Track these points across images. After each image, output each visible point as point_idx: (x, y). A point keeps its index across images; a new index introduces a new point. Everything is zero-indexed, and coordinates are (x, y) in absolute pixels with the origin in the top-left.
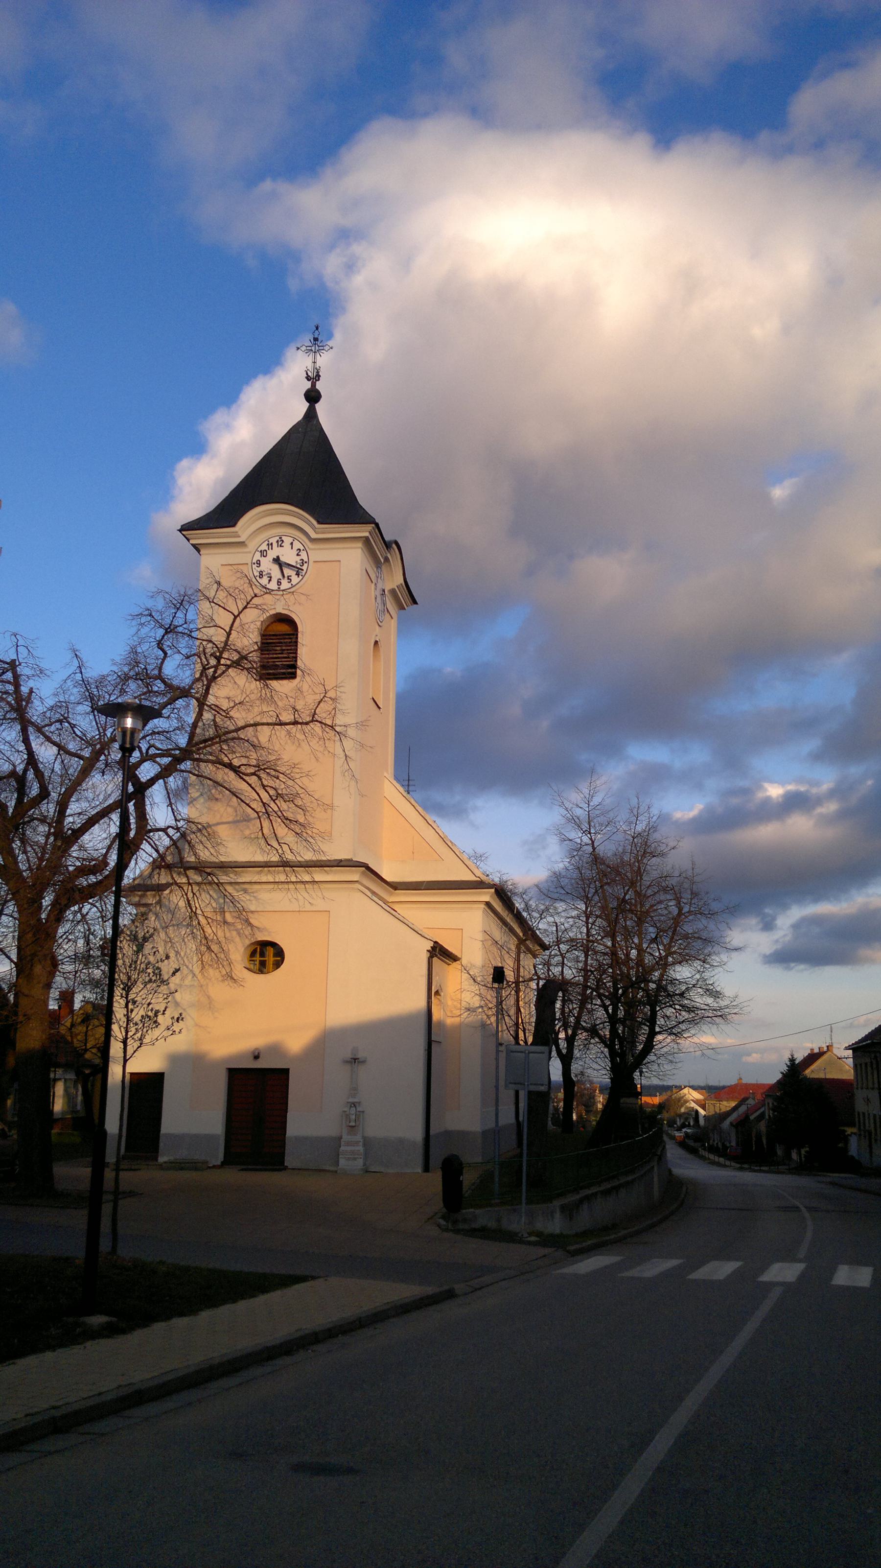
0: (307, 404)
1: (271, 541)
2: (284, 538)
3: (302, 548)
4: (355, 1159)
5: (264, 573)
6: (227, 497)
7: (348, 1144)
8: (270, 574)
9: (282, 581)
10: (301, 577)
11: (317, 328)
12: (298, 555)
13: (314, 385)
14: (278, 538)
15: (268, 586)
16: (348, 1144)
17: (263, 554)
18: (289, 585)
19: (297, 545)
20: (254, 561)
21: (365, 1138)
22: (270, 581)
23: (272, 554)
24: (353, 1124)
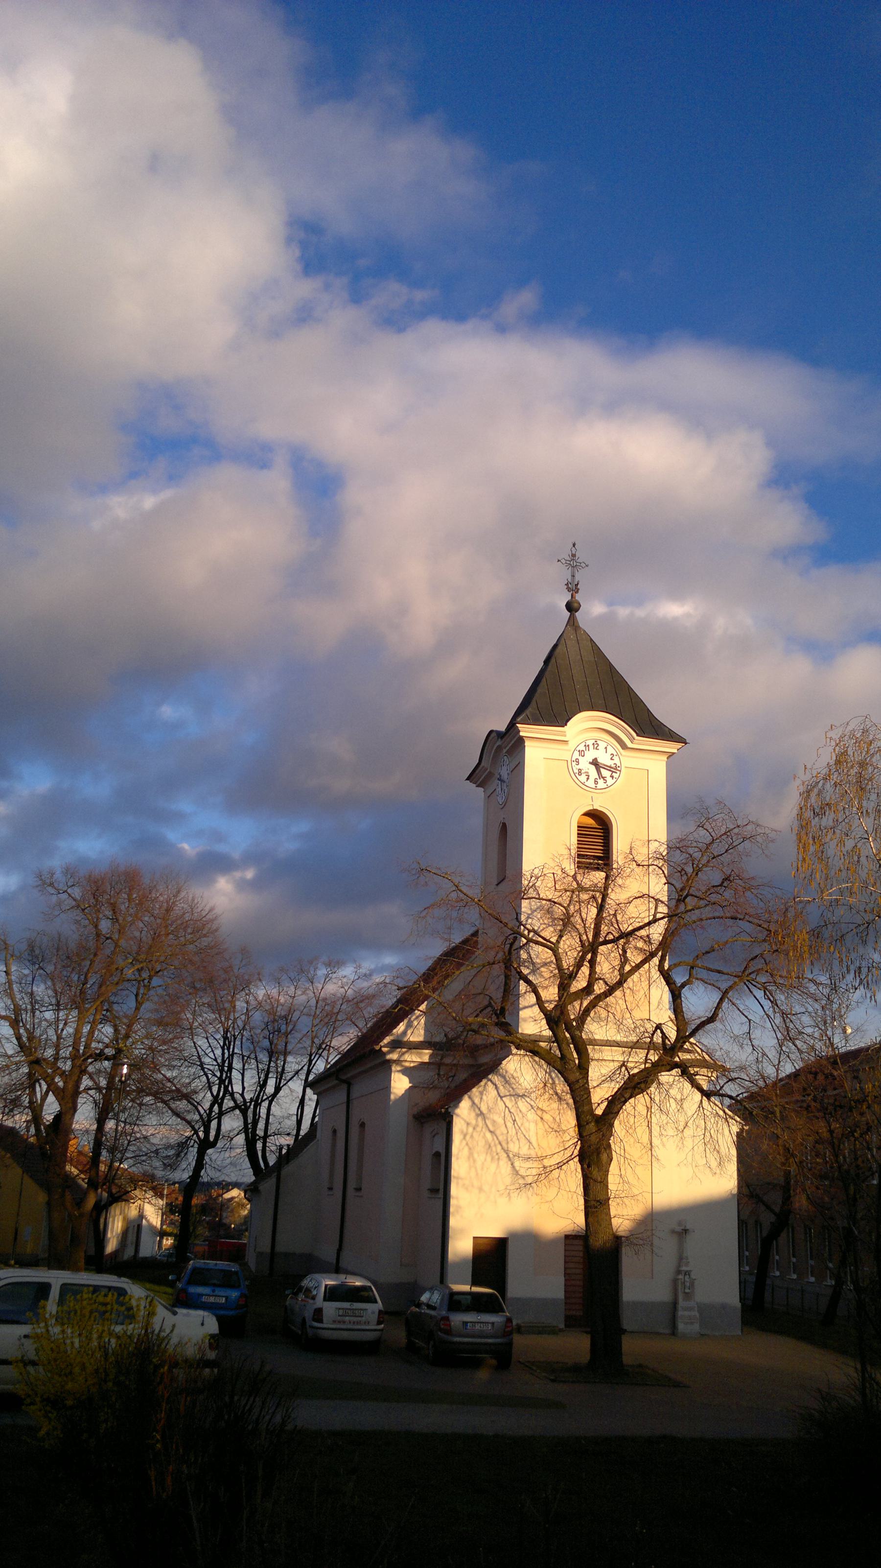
1: (588, 743)
2: (599, 742)
4: (692, 1323)
5: (582, 772)
8: (587, 772)
9: (599, 780)
10: (615, 780)
11: (574, 545)
12: (612, 759)
14: (593, 741)
15: (586, 784)
17: (582, 753)
18: (605, 786)
20: (574, 759)
22: (588, 779)
23: (591, 755)
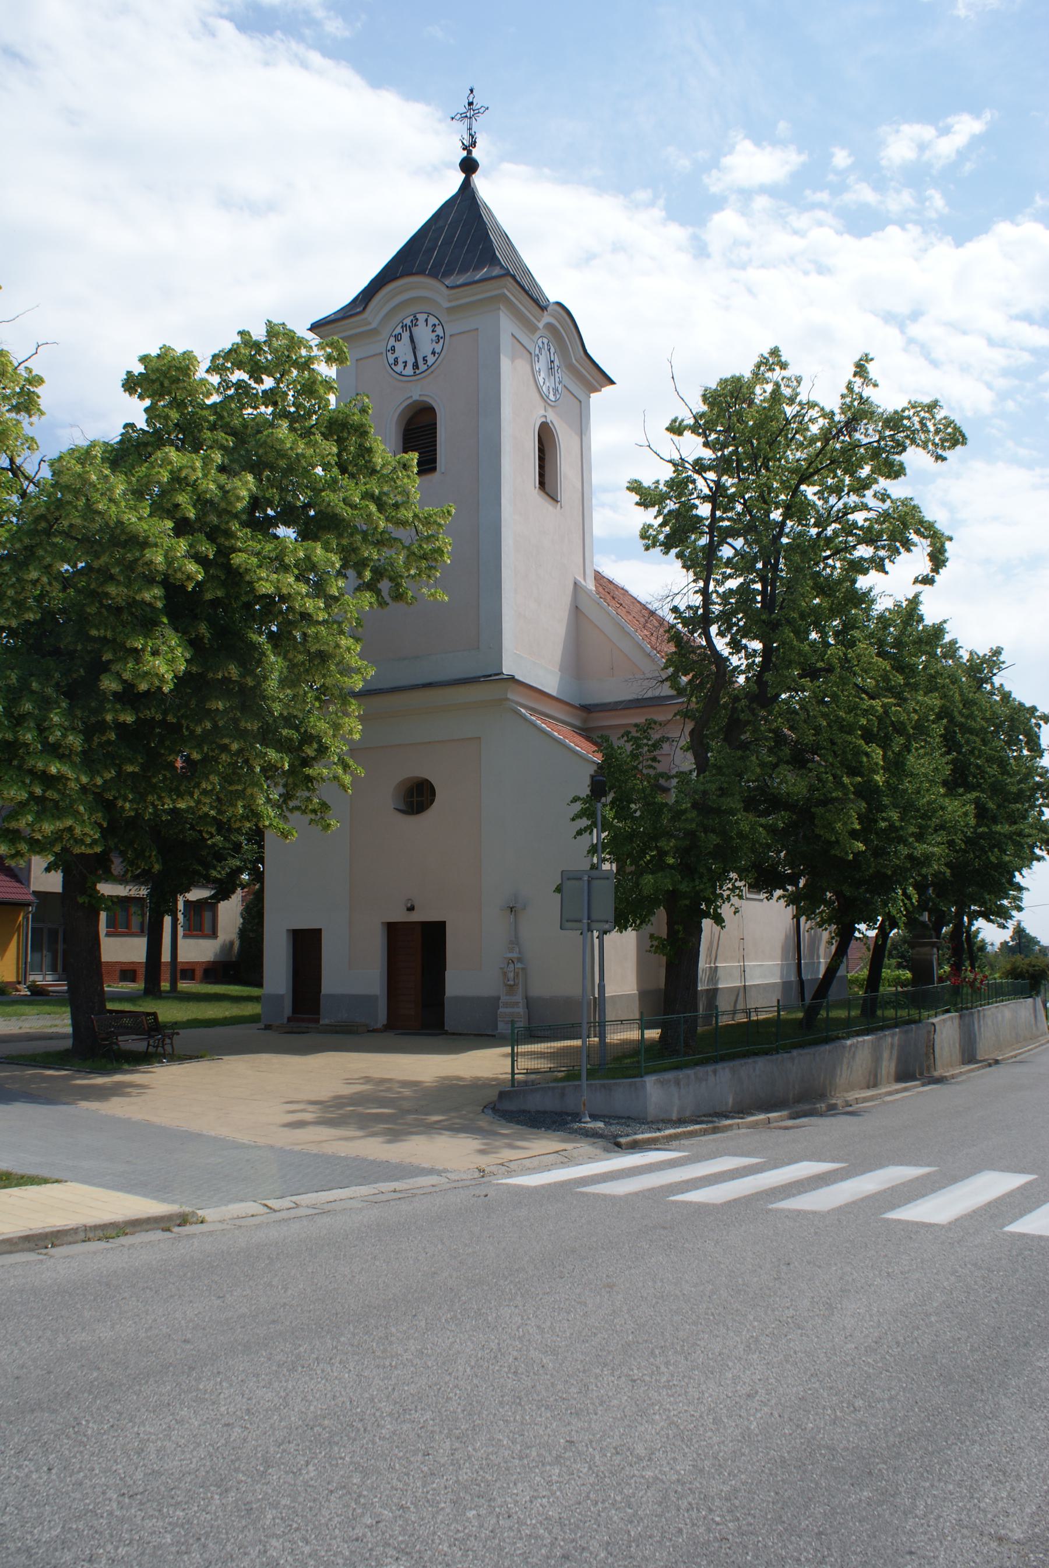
0: (463, 176)
2: (418, 316)
3: (437, 322)
6: (366, 288)
7: (507, 1005)
11: (472, 91)
13: (469, 152)
15: (404, 373)
16: (507, 1005)
18: (425, 367)
19: (432, 320)
20: (389, 348)
21: (527, 999)
24: (512, 983)
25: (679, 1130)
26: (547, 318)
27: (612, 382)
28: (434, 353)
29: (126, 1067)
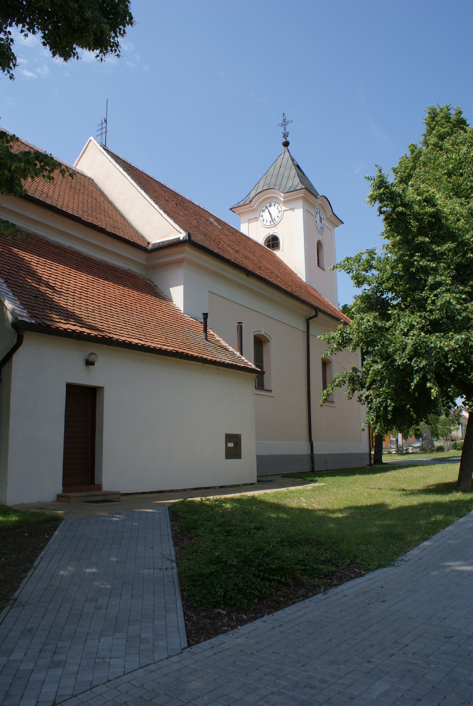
2: (271, 203)
11: (284, 115)
25: (250, 494)
26: (319, 201)
27: (343, 223)
28: (278, 217)
29: (51, 242)
